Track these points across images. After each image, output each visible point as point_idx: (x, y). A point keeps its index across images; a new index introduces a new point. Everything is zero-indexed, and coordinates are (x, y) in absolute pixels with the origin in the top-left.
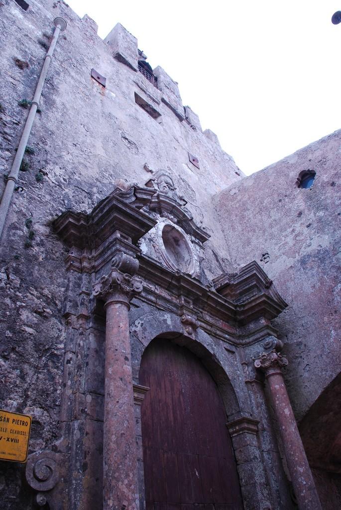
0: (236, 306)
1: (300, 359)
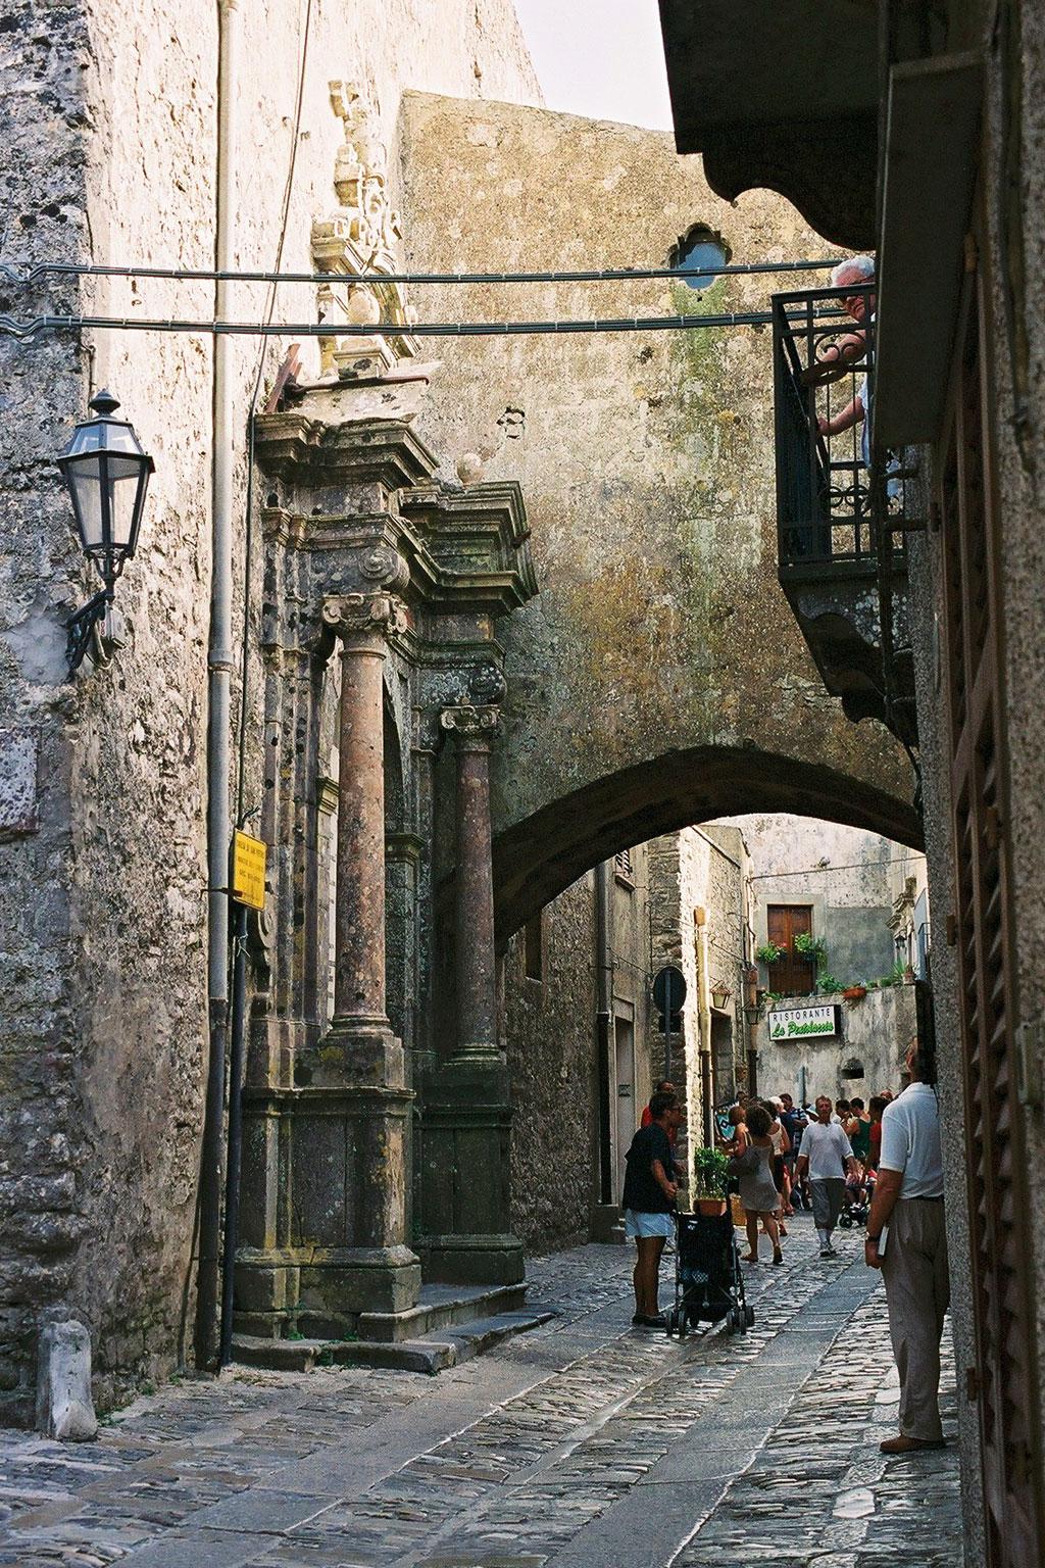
0: (439, 575)
1: (519, 720)
